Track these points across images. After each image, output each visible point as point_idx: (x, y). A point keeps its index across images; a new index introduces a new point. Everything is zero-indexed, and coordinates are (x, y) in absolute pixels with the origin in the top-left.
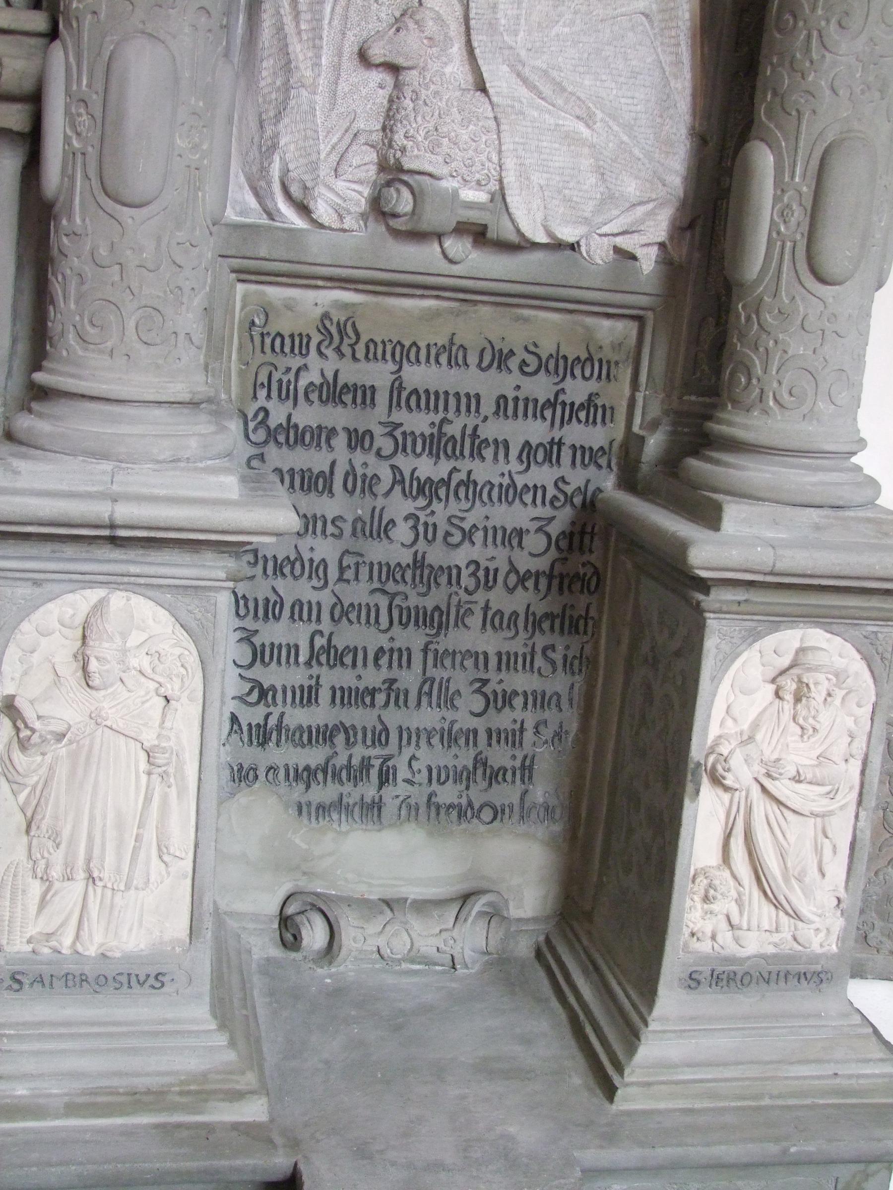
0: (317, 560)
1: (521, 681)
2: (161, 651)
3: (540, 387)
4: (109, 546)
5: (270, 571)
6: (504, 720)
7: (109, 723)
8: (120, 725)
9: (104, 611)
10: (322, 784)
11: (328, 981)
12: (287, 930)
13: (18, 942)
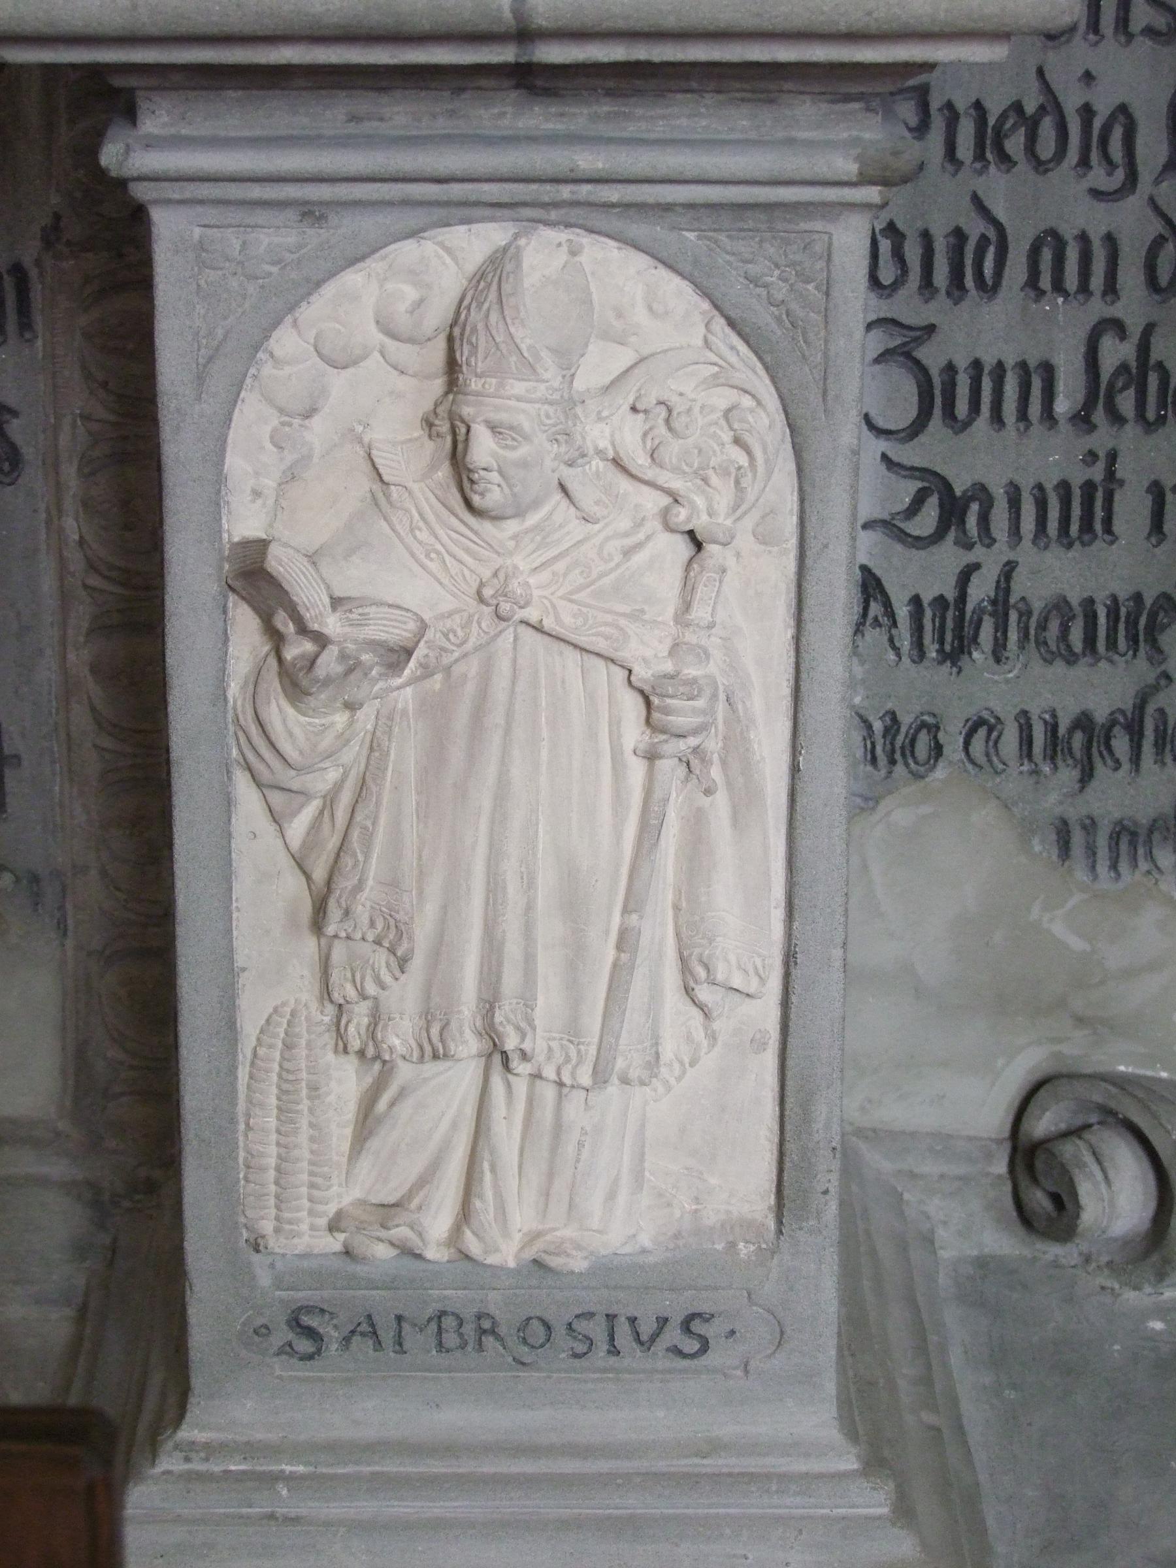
0: (1103, 110)
2: (674, 400)
4: (514, 95)
5: (965, 150)
7: (532, 614)
8: (567, 620)
9: (507, 288)
10: (1126, 766)
11: (1158, 1325)
12: (1035, 1180)
13: (304, 1227)
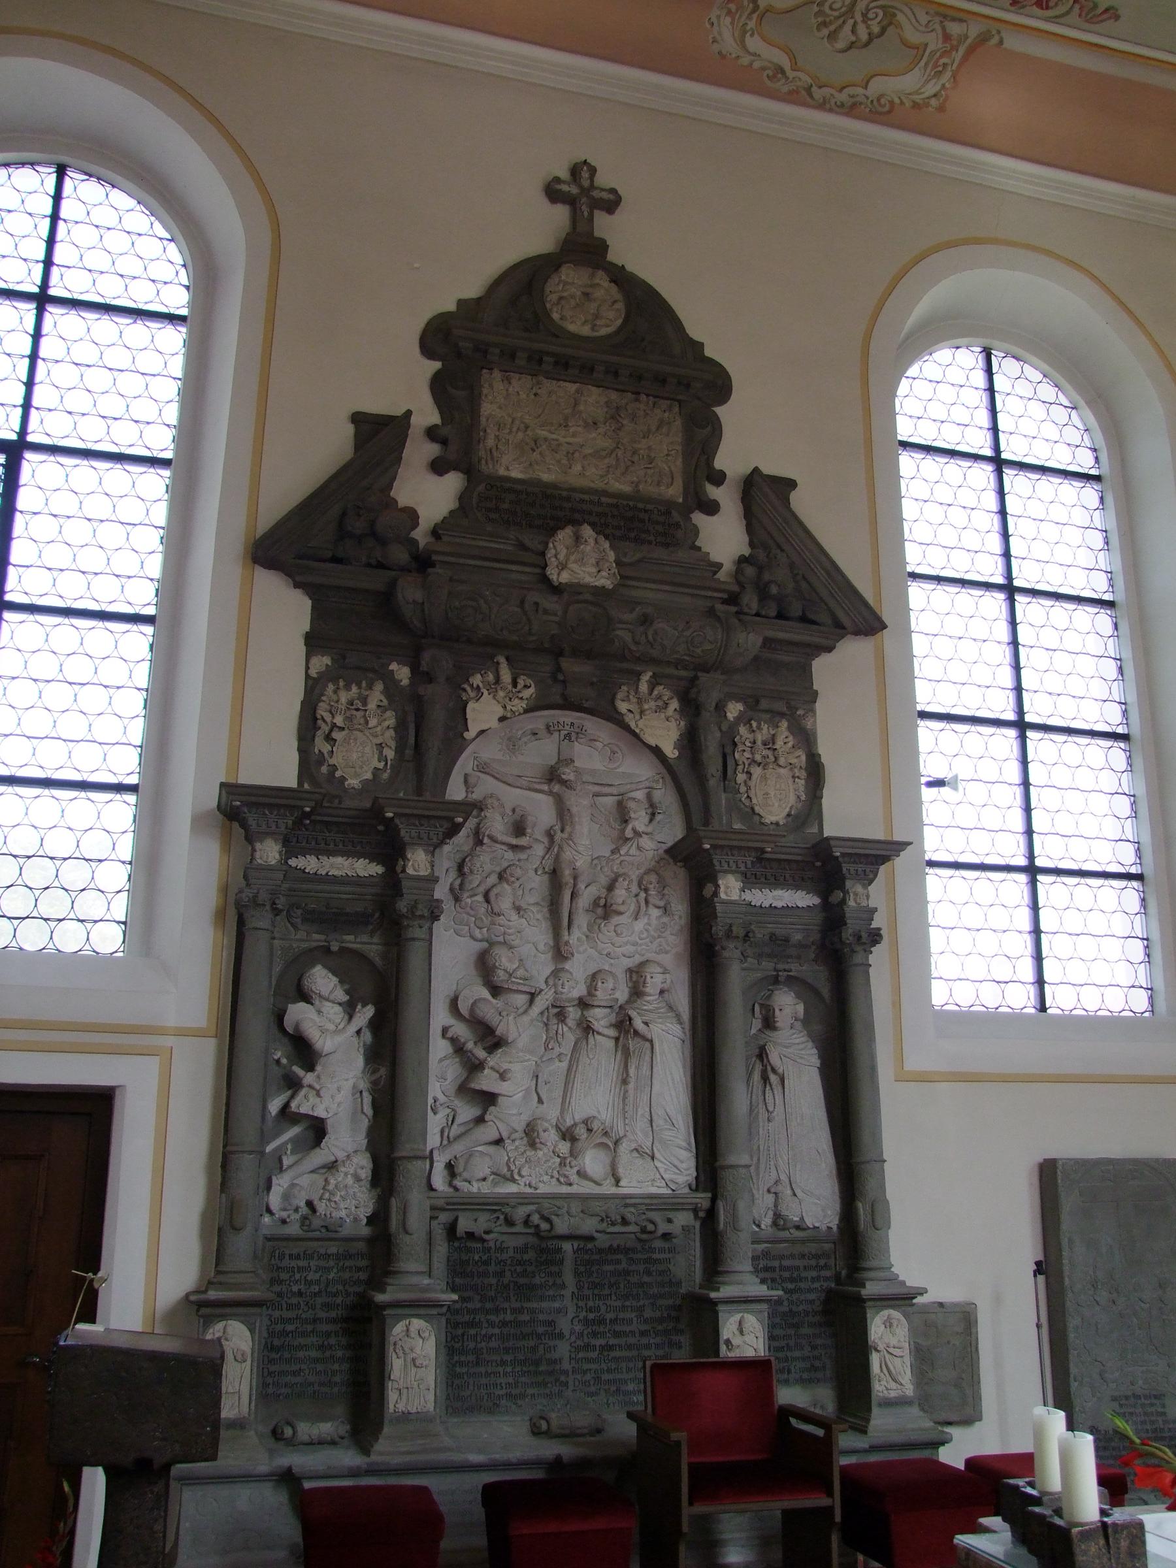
1: (819, 1342)
3: (813, 1262)
6: (816, 1353)
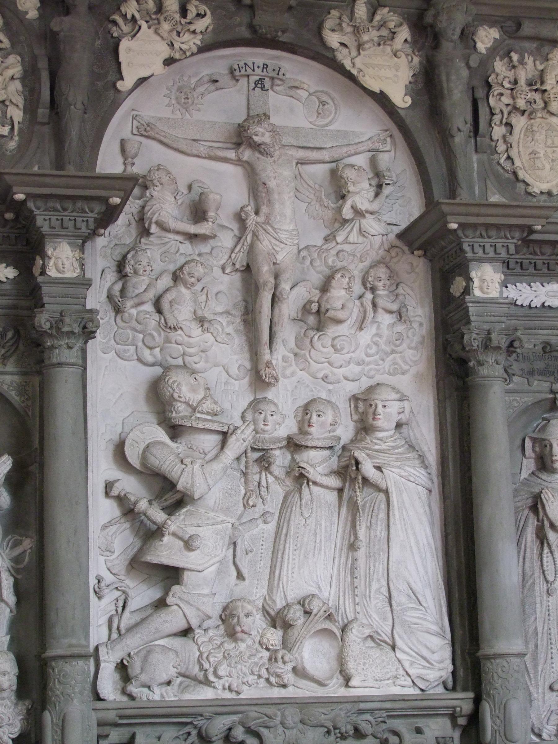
11: (98, 43)
